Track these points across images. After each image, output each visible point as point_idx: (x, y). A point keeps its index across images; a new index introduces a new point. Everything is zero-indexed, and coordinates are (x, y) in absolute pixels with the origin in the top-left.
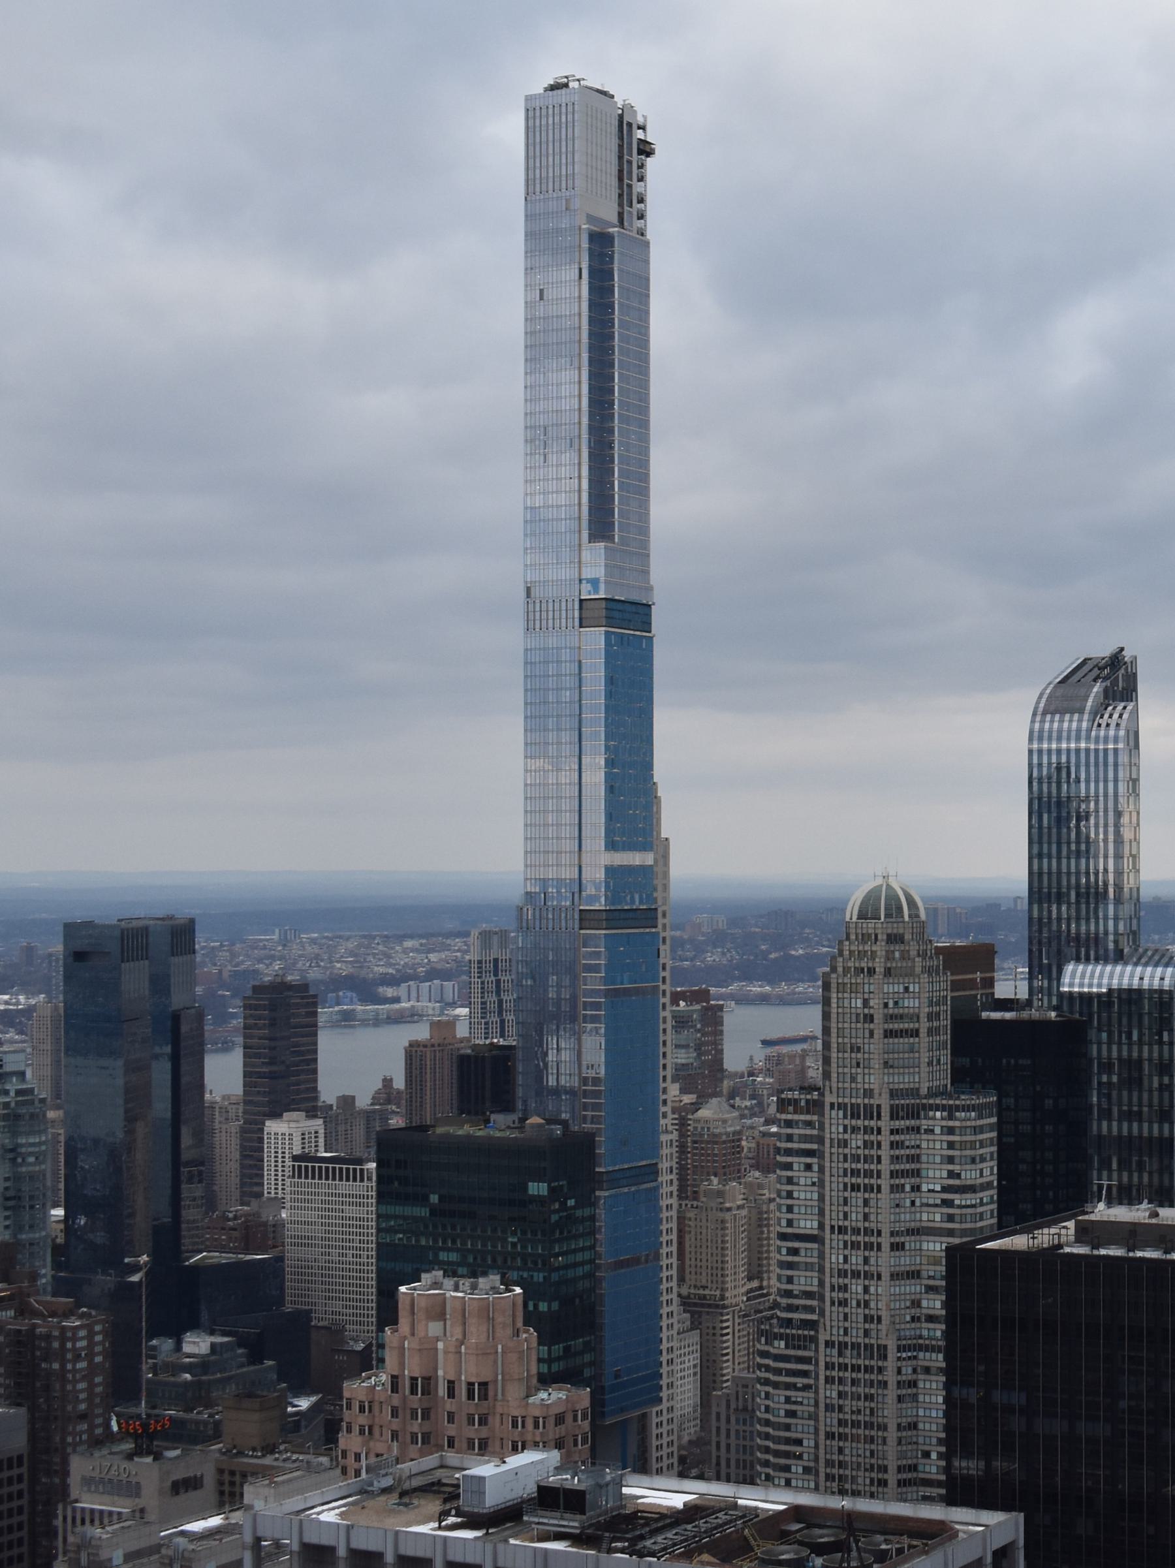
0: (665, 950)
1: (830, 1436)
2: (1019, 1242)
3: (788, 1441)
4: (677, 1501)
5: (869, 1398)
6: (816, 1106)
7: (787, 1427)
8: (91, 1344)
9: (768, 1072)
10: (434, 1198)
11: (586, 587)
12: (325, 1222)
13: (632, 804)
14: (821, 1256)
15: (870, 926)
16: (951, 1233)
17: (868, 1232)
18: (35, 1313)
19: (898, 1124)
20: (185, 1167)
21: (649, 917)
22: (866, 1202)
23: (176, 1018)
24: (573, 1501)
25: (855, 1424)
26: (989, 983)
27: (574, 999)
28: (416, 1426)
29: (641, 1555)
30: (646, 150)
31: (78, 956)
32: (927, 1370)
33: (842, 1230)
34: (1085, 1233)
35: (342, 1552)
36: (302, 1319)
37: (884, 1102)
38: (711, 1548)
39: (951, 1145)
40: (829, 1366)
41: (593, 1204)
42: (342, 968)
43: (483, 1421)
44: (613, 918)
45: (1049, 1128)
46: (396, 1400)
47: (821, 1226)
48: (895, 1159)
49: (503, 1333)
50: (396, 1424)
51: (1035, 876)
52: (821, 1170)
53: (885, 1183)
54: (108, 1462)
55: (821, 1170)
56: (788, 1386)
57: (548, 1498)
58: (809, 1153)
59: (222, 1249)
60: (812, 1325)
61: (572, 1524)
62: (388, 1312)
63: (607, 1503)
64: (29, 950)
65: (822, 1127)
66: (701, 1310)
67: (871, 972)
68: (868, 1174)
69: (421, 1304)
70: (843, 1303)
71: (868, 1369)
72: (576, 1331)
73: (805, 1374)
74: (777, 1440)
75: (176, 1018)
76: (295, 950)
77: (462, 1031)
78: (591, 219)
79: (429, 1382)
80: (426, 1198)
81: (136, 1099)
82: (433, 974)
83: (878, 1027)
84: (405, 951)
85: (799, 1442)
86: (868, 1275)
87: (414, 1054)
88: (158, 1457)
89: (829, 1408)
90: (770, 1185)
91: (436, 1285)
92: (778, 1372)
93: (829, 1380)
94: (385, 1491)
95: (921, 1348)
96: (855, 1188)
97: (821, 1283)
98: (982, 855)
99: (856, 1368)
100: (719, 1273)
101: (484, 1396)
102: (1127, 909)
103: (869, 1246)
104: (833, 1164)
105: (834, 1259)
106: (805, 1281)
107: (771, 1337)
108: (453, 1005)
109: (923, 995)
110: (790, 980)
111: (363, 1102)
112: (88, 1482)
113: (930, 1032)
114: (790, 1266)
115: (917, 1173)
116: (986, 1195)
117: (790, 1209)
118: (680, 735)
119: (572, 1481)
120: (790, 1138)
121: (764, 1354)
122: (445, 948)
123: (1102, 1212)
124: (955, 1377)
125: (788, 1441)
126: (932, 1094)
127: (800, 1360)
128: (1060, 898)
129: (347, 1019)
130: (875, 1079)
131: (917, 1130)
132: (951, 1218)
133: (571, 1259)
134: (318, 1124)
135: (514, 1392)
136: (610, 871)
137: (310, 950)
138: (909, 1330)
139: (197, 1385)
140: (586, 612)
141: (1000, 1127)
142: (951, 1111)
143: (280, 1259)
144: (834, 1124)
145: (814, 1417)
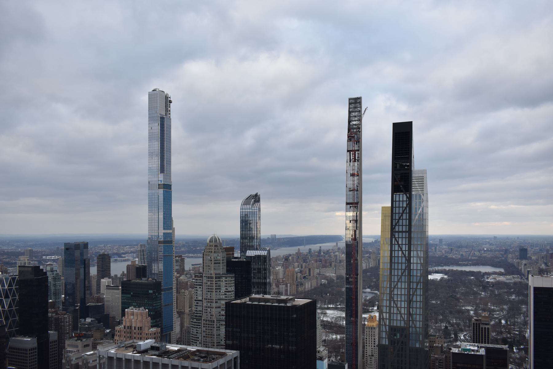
0: (174, 248)
1: (204, 337)
2: (239, 301)
4: (176, 349)
5: (211, 330)
6: (201, 277)
9: (193, 270)
12: (112, 298)
16: (226, 300)
18: (59, 314)
20: (86, 287)
21: (171, 242)
23: (85, 260)
24: (157, 349)
26: (233, 254)
28: (128, 335)
30: (170, 102)
31: (67, 249)
34: (251, 300)
36: (108, 315)
37: (214, 276)
38: (182, 357)
40: (204, 324)
41: (161, 294)
42: (115, 251)
43: (141, 334)
44: (164, 242)
48: (216, 286)
49: (144, 318)
50: (125, 335)
51: (241, 234)
53: (214, 290)
57: (153, 348)
58: (200, 285)
60: (201, 316)
61: (157, 353)
62: (123, 314)
63: (163, 349)
64: (58, 248)
66: (181, 314)
67: (212, 252)
68: (211, 289)
69: (129, 313)
70: (206, 312)
72: (158, 318)
75: (85, 260)
76: (106, 248)
77: (137, 263)
78: (160, 114)
79: (131, 327)
81: (77, 275)
82: (132, 252)
86: (211, 307)
87: (128, 267)
88: (81, 341)
89: (204, 332)
90: (193, 291)
91: (132, 309)
98: (231, 231)
101: (141, 329)
102: (258, 240)
104: (205, 287)
105: (205, 304)
106: (199, 308)
107: (193, 319)
109: (221, 256)
111: (119, 276)
112: (68, 345)
118: (176, 209)
123: (254, 296)
124: (227, 326)
126: (223, 274)
129: (116, 260)
130: (212, 272)
132: (226, 297)
134: (111, 280)
135: (147, 329)
136: (164, 233)
138: (218, 317)
139: (88, 327)
140: (160, 186)
141: (235, 280)
142: (226, 278)
143: (104, 304)
145: (201, 333)
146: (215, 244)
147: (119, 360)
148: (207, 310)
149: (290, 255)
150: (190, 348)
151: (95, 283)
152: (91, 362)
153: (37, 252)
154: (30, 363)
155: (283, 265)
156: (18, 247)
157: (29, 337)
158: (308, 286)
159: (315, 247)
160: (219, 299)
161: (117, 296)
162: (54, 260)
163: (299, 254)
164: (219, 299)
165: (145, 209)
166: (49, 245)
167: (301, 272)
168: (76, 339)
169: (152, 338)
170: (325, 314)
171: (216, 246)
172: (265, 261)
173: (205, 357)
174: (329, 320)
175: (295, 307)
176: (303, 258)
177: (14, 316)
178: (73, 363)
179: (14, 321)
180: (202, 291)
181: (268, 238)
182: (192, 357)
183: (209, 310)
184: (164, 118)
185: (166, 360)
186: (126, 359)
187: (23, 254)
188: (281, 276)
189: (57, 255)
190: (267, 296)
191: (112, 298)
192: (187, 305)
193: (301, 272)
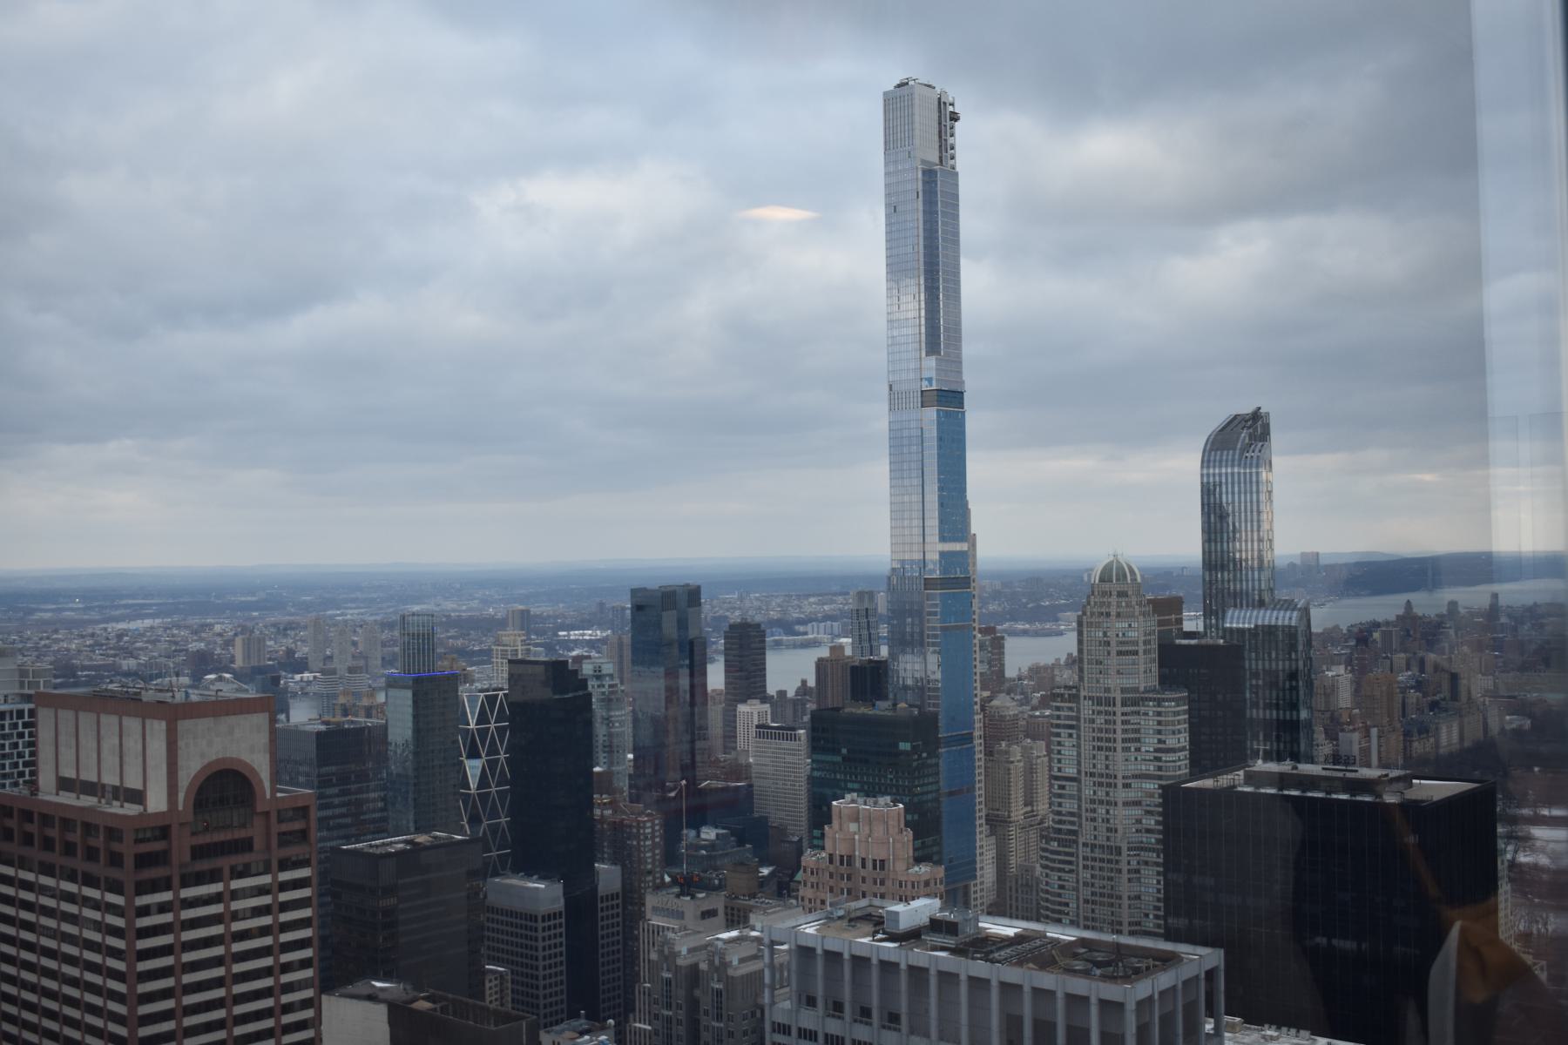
0: (976, 602)
1: (1086, 901)
2: (1208, 783)
3: (1060, 904)
4: (1011, 932)
5: (1110, 879)
6: (1075, 698)
7: (1059, 895)
8: (654, 831)
9: (1031, 678)
10: (844, 751)
11: (925, 383)
12: (778, 767)
13: (954, 515)
14: (1079, 790)
15: (1106, 587)
16: (1160, 778)
17: (1108, 776)
18: (624, 812)
19: (1126, 709)
20: (695, 730)
21: (966, 582)
22: (1107, 758)
23: (691, 643)
24: (950, 928)
25: (1102, 895)
26: (1180, 621)
27: (922, 633)
28: (844, 884)
29: (993, 961)
30: (954, 117)
31: (638, 608)
32: (1146, 863)
33: (1092, 775)
34: (1250, 778)
35: (819, 951)
36: (763, 821)
37: (1119, 697)
38: (1034, 960)
39: (1159, 723)
40: (1085, 858)
41: (937, 757)
42: (774, 615)
43: (882, 883)
44: (945, 583)
45: (1220, 713)
46: (832, 868)
47: (1079, 772)
48: (1125, 731)
49: (893, 831)
50: (832, 882)
51: (1207, 553)
52: (1079, 737)
53: (1119, 745)
54: (668, 899)
55: (1079, 737)
56: (1060, 870)
57: (936, 925)
58: (1071, 727)
59: (717, 778)
60: (1074, 833)
61: (950, 941)
62: (820, 815)
63: (970, 930)
64: (601, 605)
65: (1079, 711)
66: (997, 823)
67: (1108, 615)
68: (1108, 740)
69: (844, 812)
70: (1093, 820)
71: (1110, 861)
72: (928, 832)
73: (1070, 863)
74: (1054, 903)
75: (691, 643)
76: (747, 604)
77: (848, 652)
78: (923, 162)
79: (851, 858)
80: (838, 752)
81: (672, 692)
82: (828, 618)
83: (1114, 649)
84: (810, 604)
85: (1067, 905)
86: (1109, 803)
87: (821, 665)
88: (693, 897)
89: (1086, 884)
90: (1040, 748)
91: (853, 801)
92: (1054, 861)
93: (1085, 867)
94: (840, 918)
95: (1142, 849)
96: (1100, 749)
97: (1079, 807)
98: (1175, 542)
99: (1102, 860)
100: (1007, 803)
101: (882, 868)
102: (1265, 575)
103: (1109, 785)
104: (1086, 731)
105: (1088, 792)
106: (1069, 806)
107: (1048, 840)
108: (839, 636)
109: (1139, 629)
110: (1041, 621)
111: (791, 694)
112: (655, 909)
113: (1145, 652)
114: (1060, 796)
115: (1138, 740)
116: (1182, 754)
117: (1059, 761)
118: (983, 470)
119: (947, 915)
120: (1059, 717)
121: (1044, 850)
122: (832, 602)
123: (1260, 765)
124: (1168, 867)
125: (1060, 904)
126: (1146, 691)
127: (1067, 854)
128: (1223, 567)
129: (778, 644)
130: (1114, 682)
131: (1138, 713)
132: (1160, 769)
133: (925, 789)
134: (767, 707)
135: (901, 866)
136: (942, 554)
137: (756, 603)
138: (1136, 837)
139: (709, 857)
140: (926, 399)
141: (1189, 712)
142: (1159, 702)
143: (751, 786)
144: (1087, 709)
145: (1076, 889)
146: (1108, 592)
147: (833, 957)
148: (1094, 811)
149: (1376, 625)
150: (1055, 933)
151: (720, 717)
152: (735, 963)
153: (540, 616)
154: (544, 958)
155: (1349, 662)
156: (485, 602)
157: (542, 878)
158: (1449, 736)
159: (1472, 597)
160: (1135, 777)
161: (789, 759)
162: (591, 644)
163: (1408, 620)
164: (1135, 777)
165: (877, 473)
166: (580, 594)
167: (1419, 686)
168: (676, 890)
169: (927, 895)
170: (1528, 838)
171: (1121, 594)
172: (1293, 647)
173: (1107, 964)
174: (1544, 860)
175: (1413, 810)
176: (1420, 633)
177: (494, 814)
178: (680, 962)
179: (494, 829)
180: (1079, 746)
181: (1292, 566)
182: (1063, 962)
183: (1101, 810)
184: (935, 172)
185: (979, 968)
186: (854, 958)
187: (502, 624)
188: (1344, 698)
189: (601, 626)
190: (1306, 768)
191: (778, 767)
192: (1017, 795)
193: (1419, 686)
